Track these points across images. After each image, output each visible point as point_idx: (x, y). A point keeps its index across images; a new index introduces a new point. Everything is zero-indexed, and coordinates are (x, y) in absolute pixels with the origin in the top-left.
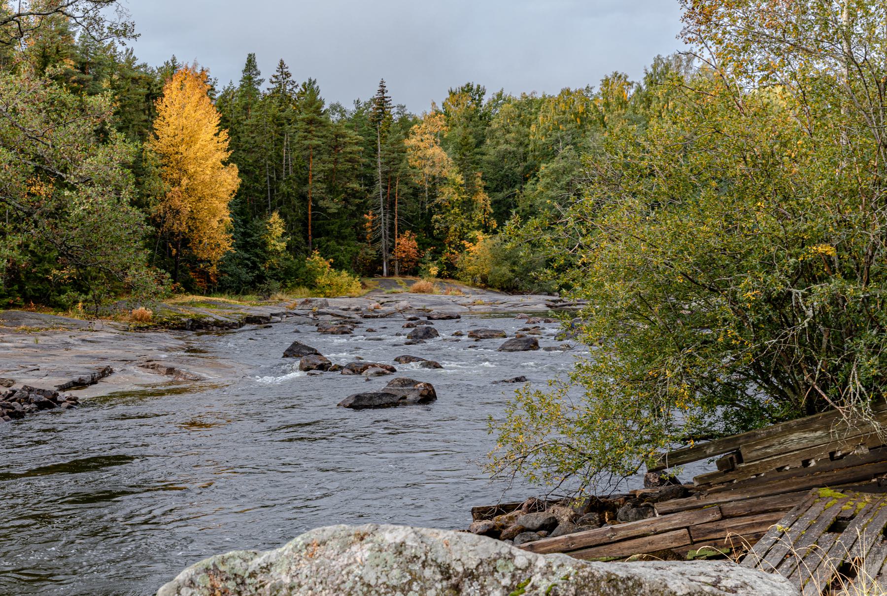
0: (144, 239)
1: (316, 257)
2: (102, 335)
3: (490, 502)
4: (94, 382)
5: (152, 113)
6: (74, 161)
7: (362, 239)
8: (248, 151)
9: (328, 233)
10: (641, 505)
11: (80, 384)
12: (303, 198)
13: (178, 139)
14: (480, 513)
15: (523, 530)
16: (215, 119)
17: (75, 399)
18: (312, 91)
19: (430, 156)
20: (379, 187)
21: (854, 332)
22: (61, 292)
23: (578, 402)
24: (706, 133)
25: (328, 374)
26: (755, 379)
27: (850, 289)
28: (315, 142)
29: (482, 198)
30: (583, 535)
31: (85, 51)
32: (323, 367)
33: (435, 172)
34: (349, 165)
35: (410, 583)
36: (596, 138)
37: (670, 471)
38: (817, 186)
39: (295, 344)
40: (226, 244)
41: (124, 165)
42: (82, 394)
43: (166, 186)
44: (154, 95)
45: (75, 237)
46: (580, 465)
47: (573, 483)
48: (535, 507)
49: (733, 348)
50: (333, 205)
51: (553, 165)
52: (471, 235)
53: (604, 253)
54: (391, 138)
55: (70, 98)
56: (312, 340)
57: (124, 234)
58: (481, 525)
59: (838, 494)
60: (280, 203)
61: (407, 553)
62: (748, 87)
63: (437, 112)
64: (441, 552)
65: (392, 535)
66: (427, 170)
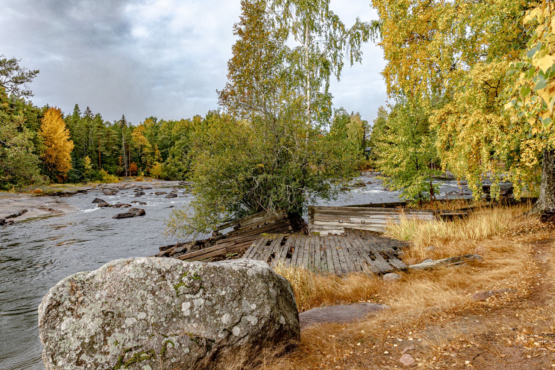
0: (38, 165)
1: (102, 170)
2: (23, 199)
3: (166, 245)
4: (20, 215)
5: (40, 123)
6: (9, 138)
7: (118, 164)
8: (77, 136)
9: (106, 163)
10: (212, 242)
11: (14, 216)
12: (97, 151)
13: (50, 132)
14: (162, 249)
15: (176, 253)
16: (64, 126)
17: (13, 221)
18: (99, 117)
19: (140, 139)
20: (123, 148)
21: (270, 188)
22: (5, 184)
23: (192, 213)
24: (227, 132)
25: (107, 208)
26: (243, 203)
27: (269, 176)
28: (101, 133)
29: (158, 152)
30: (195, 252)
31: (12, 100)
32: (106, 206)
33: (142, 143)
34: (113, 141)
35: (147, 277)
36: (192, 134)
37: (220, 231)
38: (259, 147)
39: (96, 199)
40: (70, 167)
41: (29, 139)
42: (15, 220)
43: (46, 148)
44: (40, 117)
45: (11, 165)
46: (193, 232)
47: (191, 237)
48: (179, 245)
49: (237, 194)
50: (108, 154)
51: (179, 142)
52: (154, 163)
53: (199, 167)
54: (127, 133)
55: (6, 116)
56: (102, 197)
57: (30, 164)
58: (163, 252)
59: (268, 235)
60: (89, 153)
61: (146, 266)
62: (238, 119)
63: (142, 125)
64: (158, 265)
65: (140, 260)
66: (139, 143)
